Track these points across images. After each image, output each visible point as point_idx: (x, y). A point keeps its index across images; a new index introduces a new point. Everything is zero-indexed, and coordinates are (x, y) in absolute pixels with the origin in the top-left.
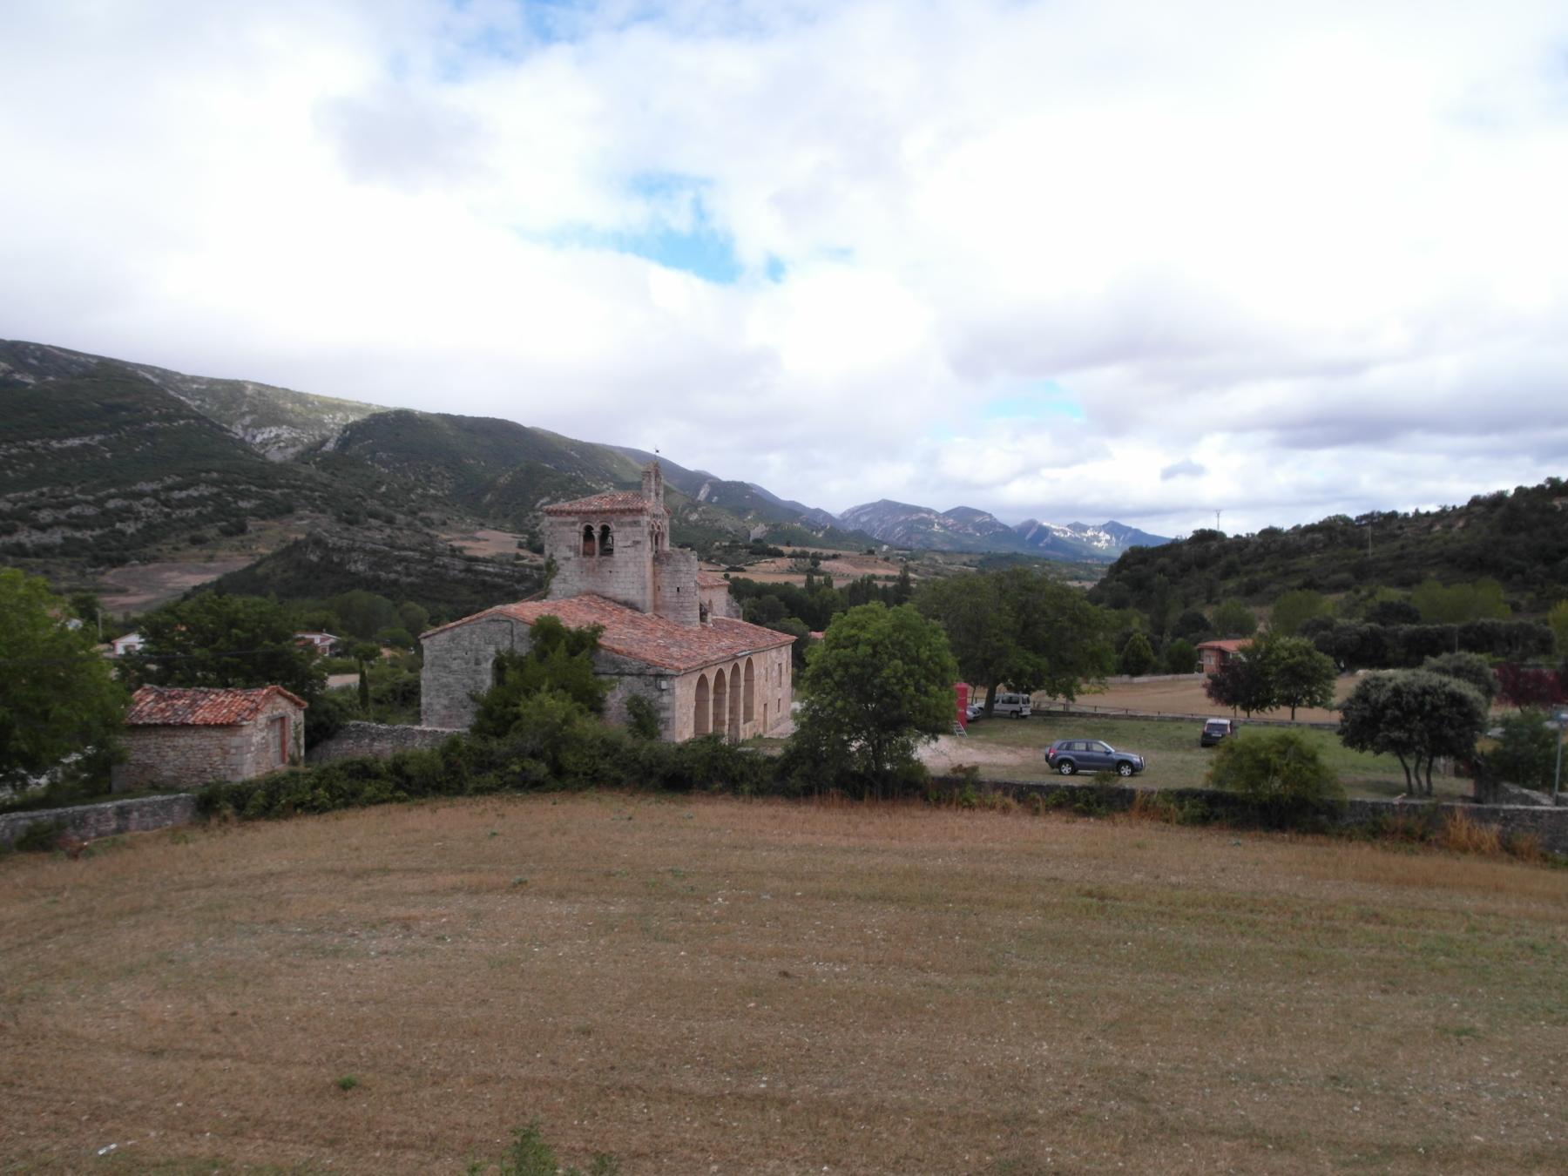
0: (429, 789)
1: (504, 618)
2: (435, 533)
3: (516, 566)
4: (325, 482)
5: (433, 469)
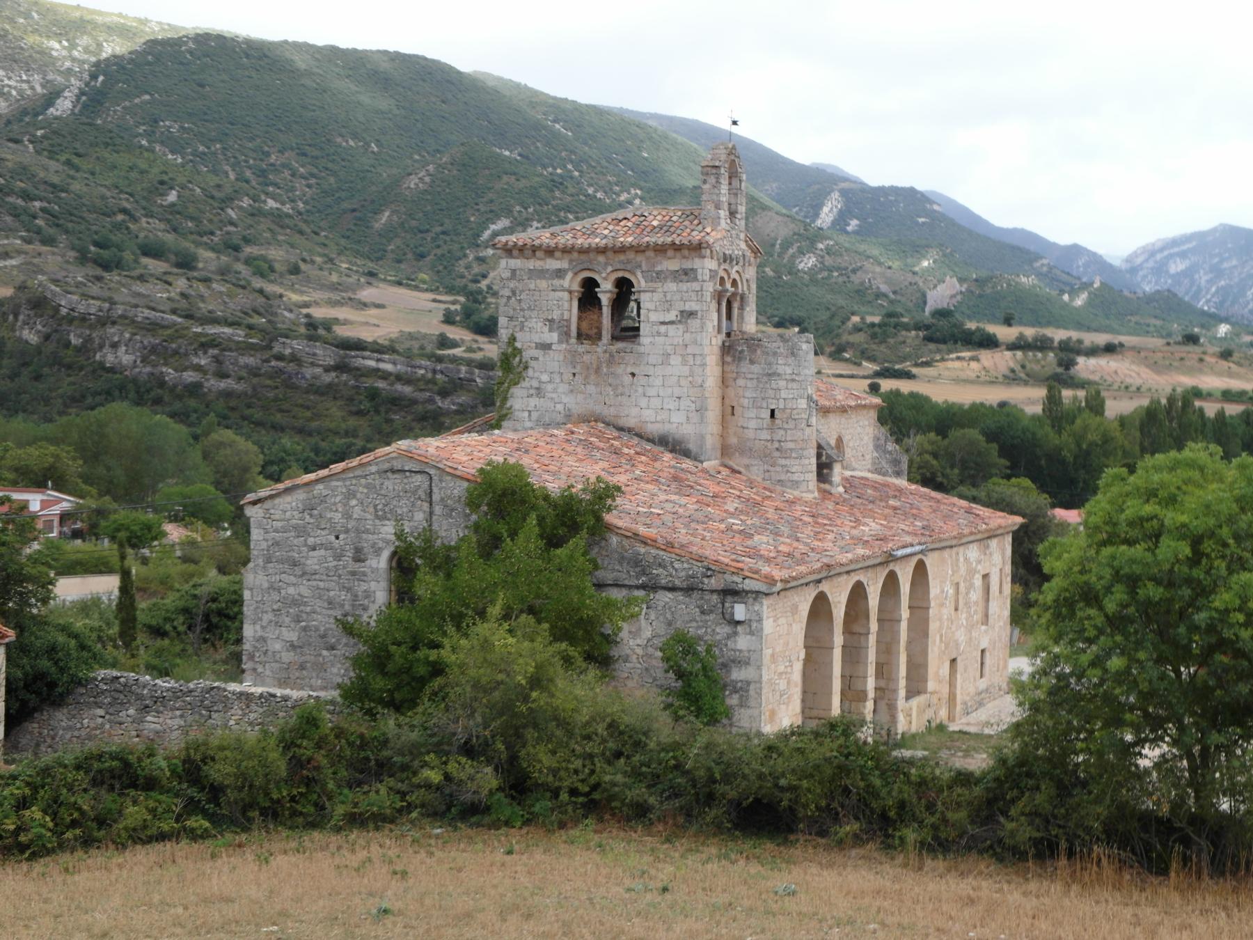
0: (255, 814)
3: (440, 359)
4: (55, 179)
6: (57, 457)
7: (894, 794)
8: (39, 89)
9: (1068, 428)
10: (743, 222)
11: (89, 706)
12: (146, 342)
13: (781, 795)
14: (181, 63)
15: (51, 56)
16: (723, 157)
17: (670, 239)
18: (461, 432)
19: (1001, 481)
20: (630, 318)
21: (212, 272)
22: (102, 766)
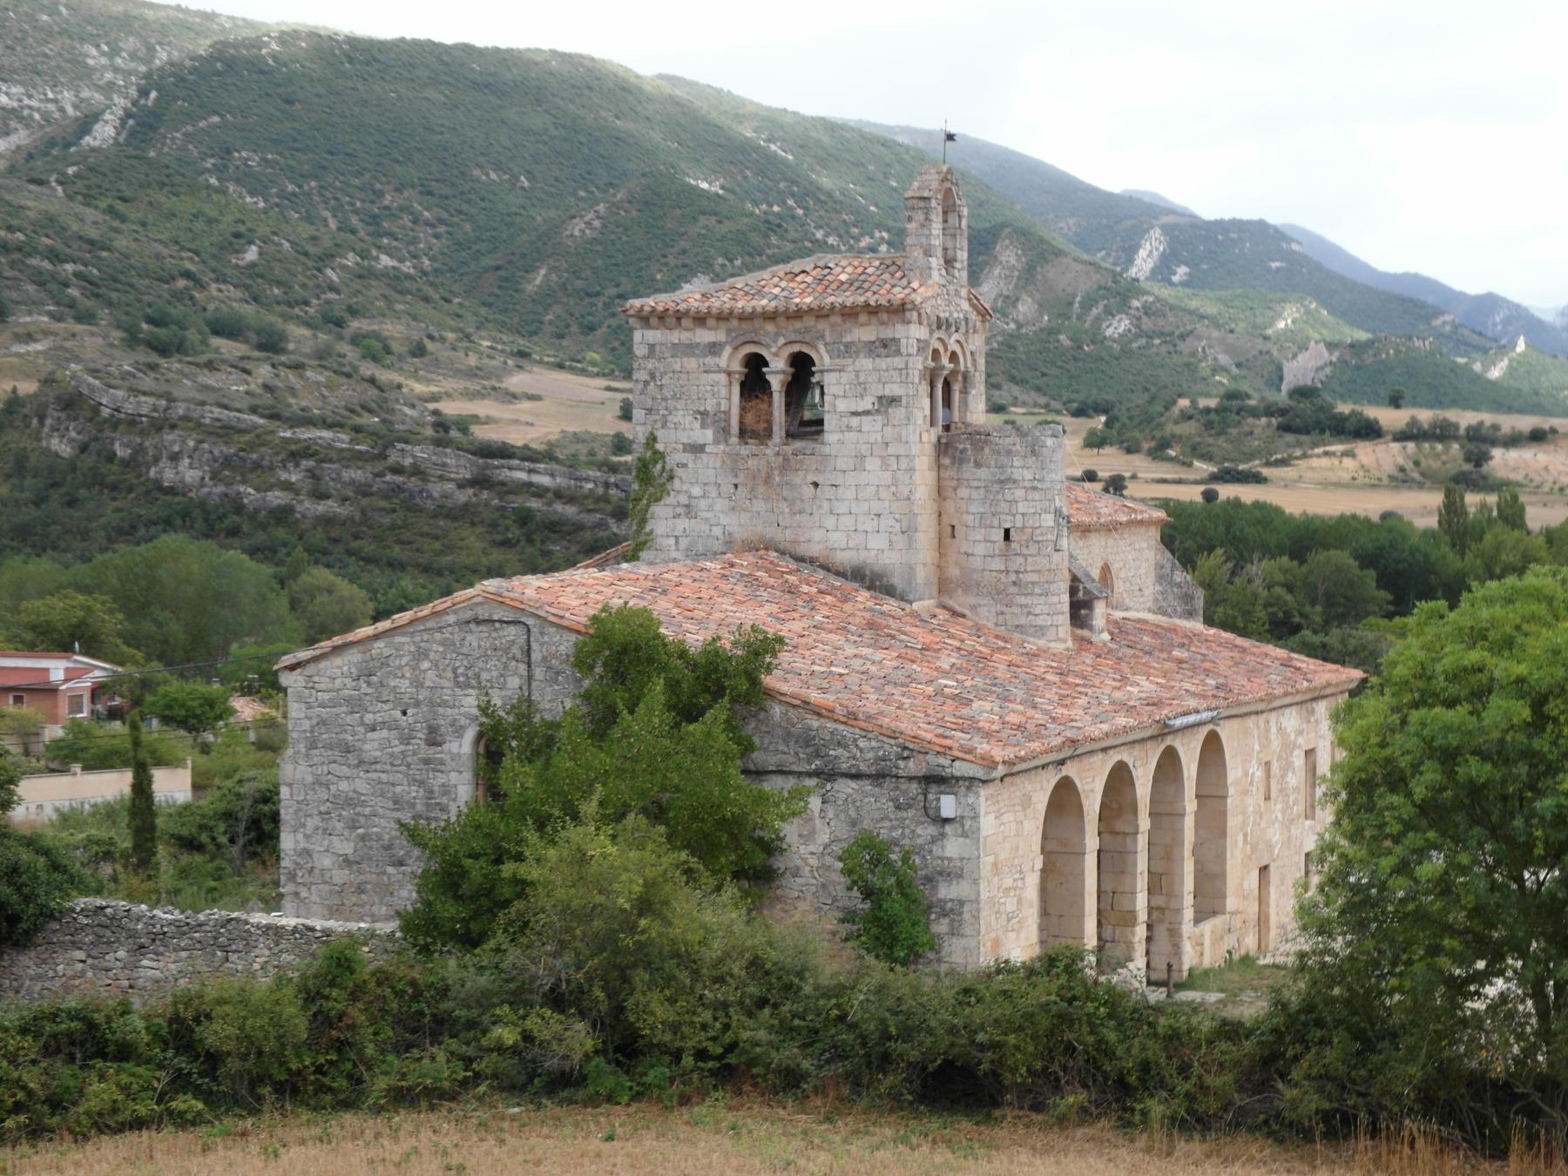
0: (266, 1091)
1: (509, 617)
3: (614, 469)
4: (93, 233)
5: (388, 198)
6: (88, 609)
8: (70, 111)
9: (1473, 546)
11: (65, 947)
12: (216, 452)
13: (979, 1055)
15: (86, 66)
16: (935, 185)
18: (587, 567)
21: (307, 356)
22: (56, 1028)
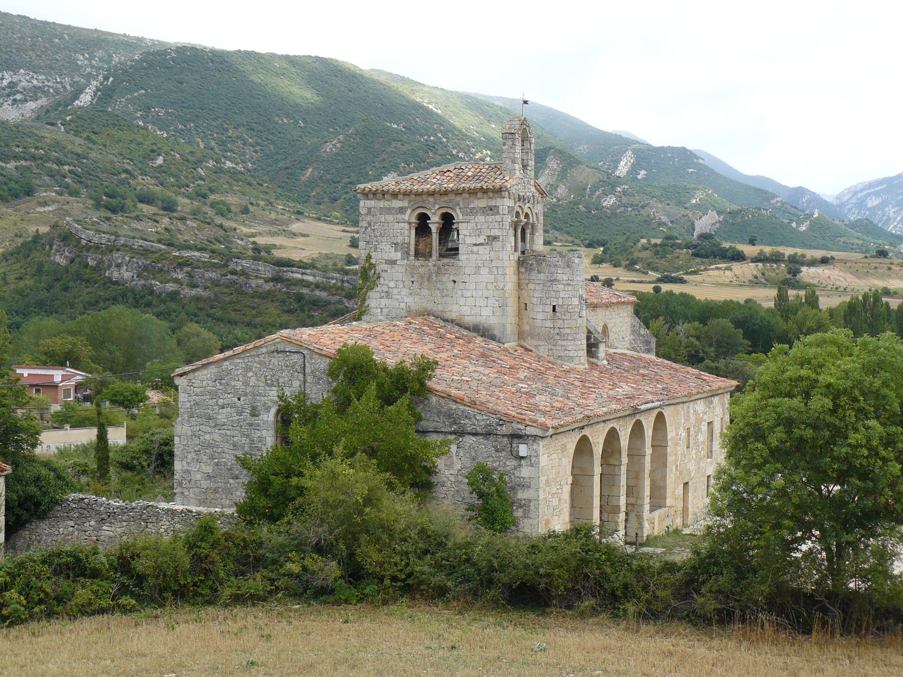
2: (233, 225)
3: (346, 273)
4: (79, 150)
7: (620, 578)
10: (533, 173)
13: (540, 580)
14: (168, 68)
16: (517, 127)
17: (480, 185)
19: (744, 355)
20: (453, 241)
21: (187, 213)
